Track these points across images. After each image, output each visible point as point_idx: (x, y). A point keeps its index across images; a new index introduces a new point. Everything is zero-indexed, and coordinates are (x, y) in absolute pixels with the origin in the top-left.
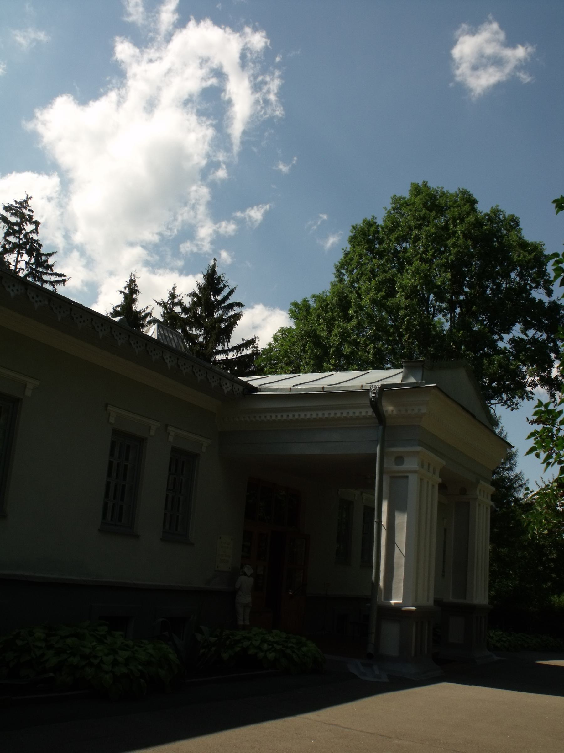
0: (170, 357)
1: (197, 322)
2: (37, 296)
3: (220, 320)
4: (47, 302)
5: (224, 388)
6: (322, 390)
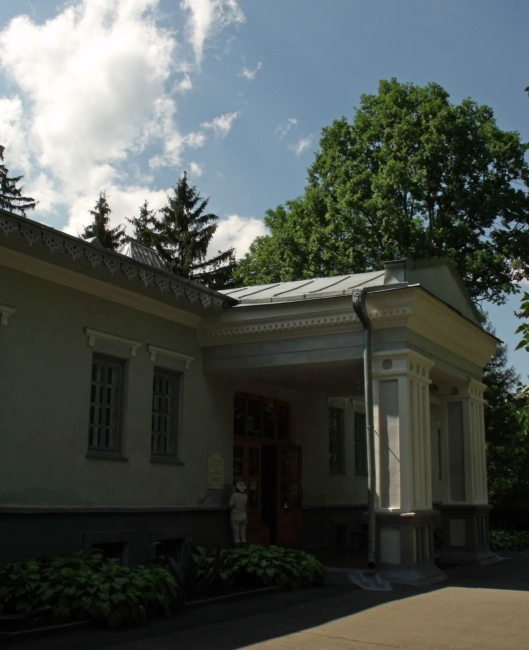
0: (146, 275)
1: (172, 237)
2: (7, 223)
3: (195, 234)
4: (17, 228)
5: (203, 302)
6: (303, 298)
